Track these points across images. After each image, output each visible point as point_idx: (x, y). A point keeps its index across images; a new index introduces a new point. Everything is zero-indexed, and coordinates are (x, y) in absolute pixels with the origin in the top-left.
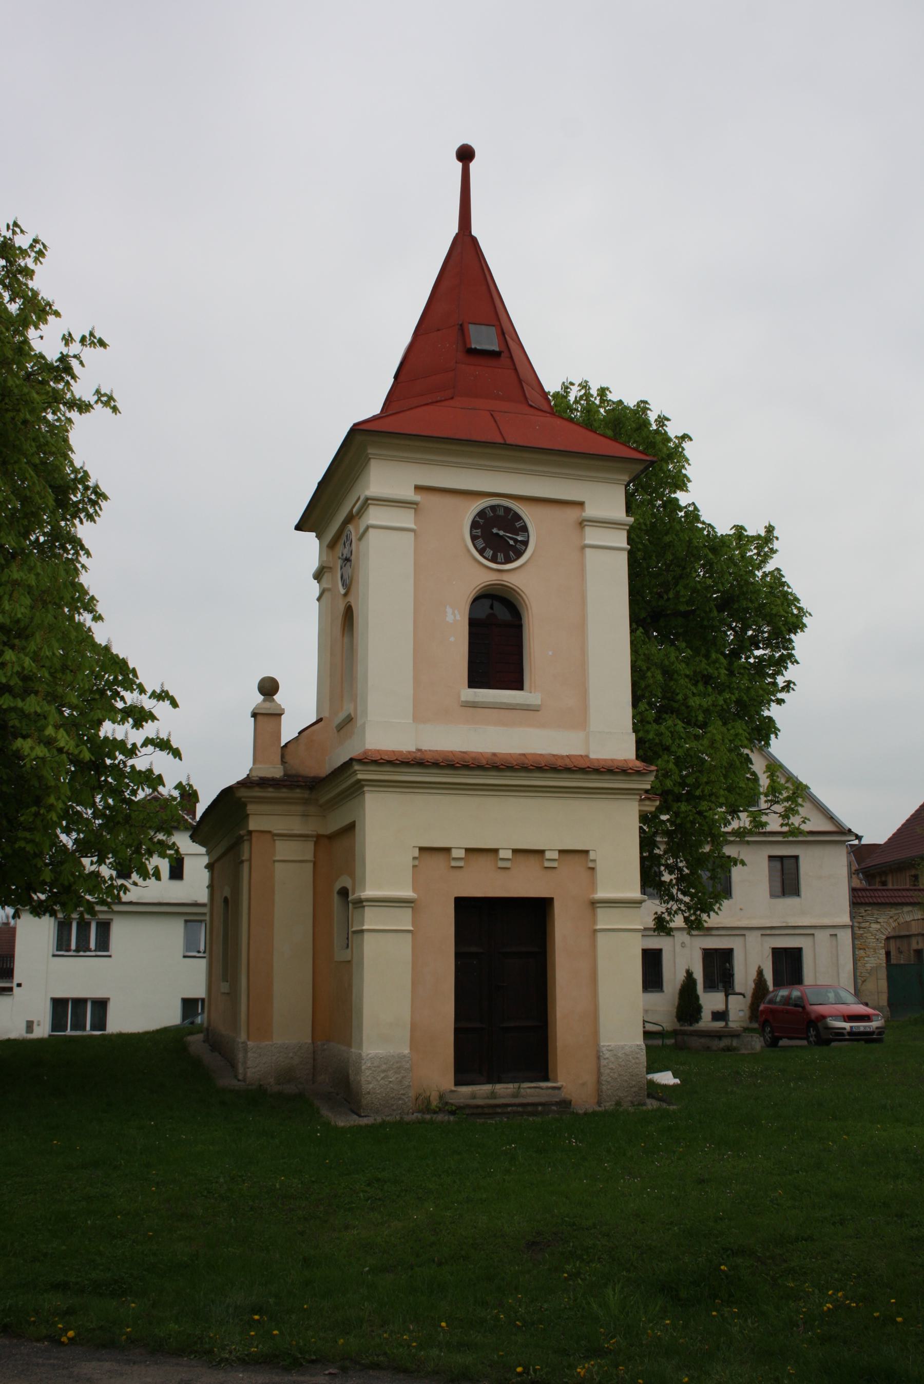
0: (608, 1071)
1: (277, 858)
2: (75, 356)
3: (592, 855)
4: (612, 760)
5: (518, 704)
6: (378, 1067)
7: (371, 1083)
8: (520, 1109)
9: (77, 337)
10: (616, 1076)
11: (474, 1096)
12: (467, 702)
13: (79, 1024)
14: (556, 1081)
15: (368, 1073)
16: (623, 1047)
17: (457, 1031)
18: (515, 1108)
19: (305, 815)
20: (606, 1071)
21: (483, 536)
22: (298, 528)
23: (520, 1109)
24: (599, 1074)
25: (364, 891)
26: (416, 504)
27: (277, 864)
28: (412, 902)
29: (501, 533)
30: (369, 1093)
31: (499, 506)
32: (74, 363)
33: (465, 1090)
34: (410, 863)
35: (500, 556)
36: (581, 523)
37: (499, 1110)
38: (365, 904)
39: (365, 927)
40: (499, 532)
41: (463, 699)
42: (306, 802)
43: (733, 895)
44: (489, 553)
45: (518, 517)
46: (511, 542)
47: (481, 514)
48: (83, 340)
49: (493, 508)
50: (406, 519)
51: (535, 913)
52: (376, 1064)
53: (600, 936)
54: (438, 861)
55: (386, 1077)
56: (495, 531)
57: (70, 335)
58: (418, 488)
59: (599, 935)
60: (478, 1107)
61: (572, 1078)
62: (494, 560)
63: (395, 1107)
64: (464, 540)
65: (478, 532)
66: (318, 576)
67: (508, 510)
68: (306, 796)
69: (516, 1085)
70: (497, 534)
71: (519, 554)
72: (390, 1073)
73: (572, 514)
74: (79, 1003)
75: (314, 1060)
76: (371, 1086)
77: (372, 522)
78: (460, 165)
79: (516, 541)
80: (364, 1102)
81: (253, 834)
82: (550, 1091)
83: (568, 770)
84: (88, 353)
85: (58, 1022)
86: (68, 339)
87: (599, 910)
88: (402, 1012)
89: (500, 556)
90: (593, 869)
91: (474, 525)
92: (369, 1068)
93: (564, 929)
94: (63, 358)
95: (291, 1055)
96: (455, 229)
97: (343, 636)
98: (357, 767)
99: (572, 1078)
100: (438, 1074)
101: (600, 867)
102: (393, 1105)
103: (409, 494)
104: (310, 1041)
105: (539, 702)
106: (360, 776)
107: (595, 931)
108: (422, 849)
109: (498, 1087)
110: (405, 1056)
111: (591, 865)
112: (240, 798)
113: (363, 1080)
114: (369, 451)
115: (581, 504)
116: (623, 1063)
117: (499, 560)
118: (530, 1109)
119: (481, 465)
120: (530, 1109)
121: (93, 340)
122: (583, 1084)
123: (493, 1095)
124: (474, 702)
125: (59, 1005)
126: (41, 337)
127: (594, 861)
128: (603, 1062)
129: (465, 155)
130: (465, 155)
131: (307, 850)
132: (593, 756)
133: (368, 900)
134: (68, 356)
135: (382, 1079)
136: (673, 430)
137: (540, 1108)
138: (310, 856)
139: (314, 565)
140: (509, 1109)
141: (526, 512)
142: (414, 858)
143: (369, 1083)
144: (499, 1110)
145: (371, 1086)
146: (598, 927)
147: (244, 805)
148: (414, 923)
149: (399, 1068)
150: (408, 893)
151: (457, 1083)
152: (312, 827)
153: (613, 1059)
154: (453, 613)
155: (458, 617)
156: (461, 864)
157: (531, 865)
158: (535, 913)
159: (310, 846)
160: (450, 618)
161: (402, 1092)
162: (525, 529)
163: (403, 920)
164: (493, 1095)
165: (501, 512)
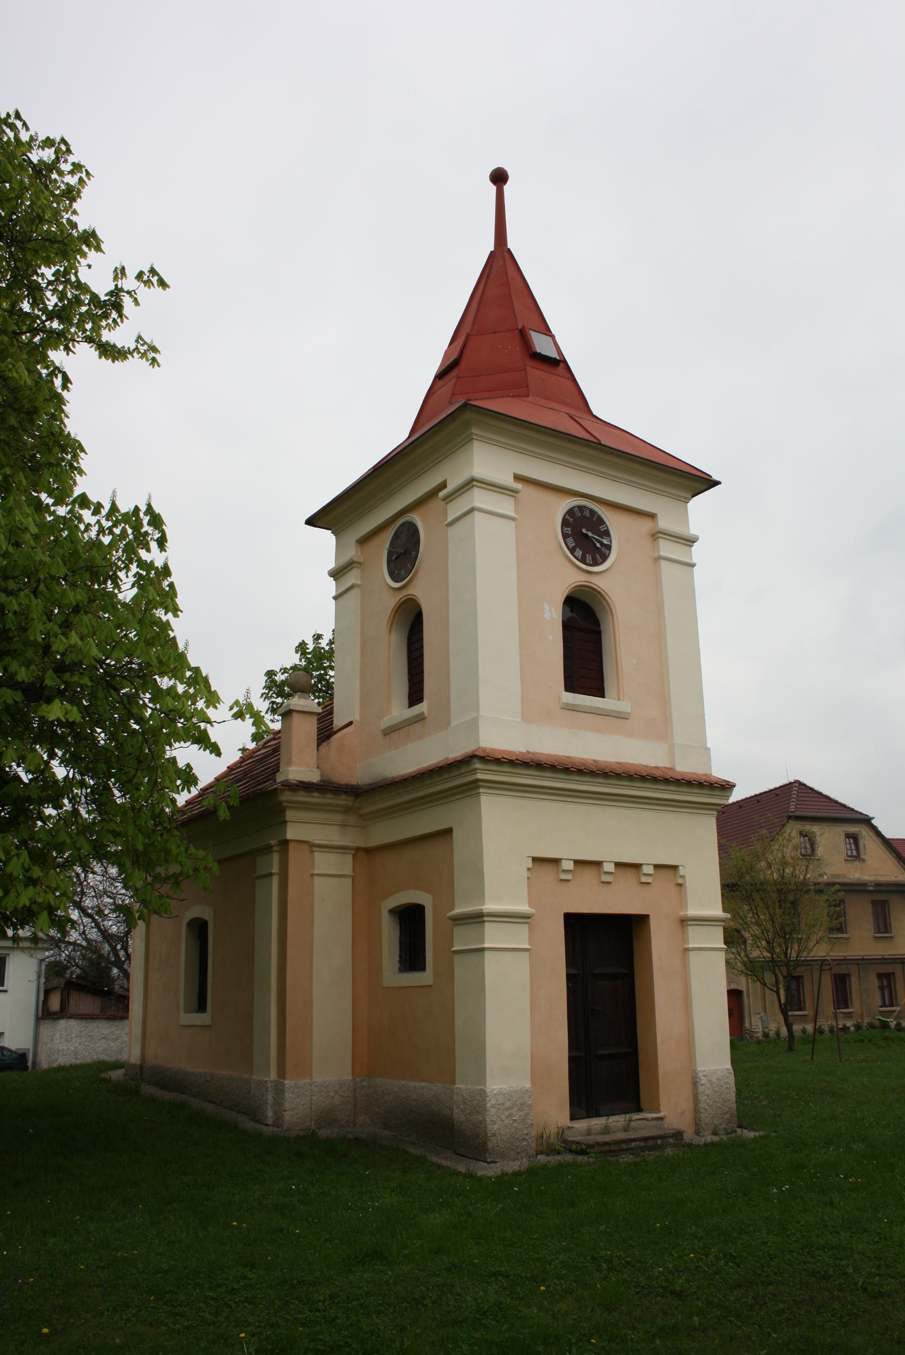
0: (705, 1097)
1: (316, 872)
2: (129, 292)
3: (681, 871)
5: (611, 710)
6: (503, 1104)
7: (497, 1124)
8: (642, 1144)
9: (132, 273)
10: (711, 1103)
12: (567, 704)
14: (659, 1111)
15: (493, 1111)
16: (715, 1072)
17: (571, 1059)
18: (638, 1143)
19: (344, 825)
20: (703, 1098)
21: (573, 535)
23: (642, 1144)
24: (696, 1100)
25: (484, 904)
26: (516, 492)
27: (315, 878)
28: (528, 918)
29: (590, 534)
30: (494, 1134)
31: (585, 507)
32: (127, 301)
33: (581, 1125)
34: (526, 874)
35: (589, 558)
36: (653, 535)
37: (624, 1146)
38: (485, 919)
39: (486, 945)
41: (564, 700)
42: (347, 810)
44: (579, 553)
45: (601, 522)
46: (598, 545)
47: (570, 512)
48: (140, 276)
49: (581, 508)
50: (505, 505)
52: (500, 1101)
53: (693, 956)
54: (547, 872)
55: (511, 1115)
56: (584, 531)
57: (123, 269)
58: (518, 478)
59: (692, 954)
62: (583, 560)
63: (519, 1150)
64: (557, 537)
65: (568, 530)
66: (336, 574)
67: (593, 512)
68: (350, 803)
69: (628, 1116)
70: (586, 535)
71: (605, 558)
72: (514, 1111)
73: (645, 525)
75: (355, 1098)
76: (496, 1126)
77: (477, 504)
78: (493, 188)
79: (602, 544)
80: (490, 1145)
81: (291, 844)
82: (654, 1122)
84: (143, 292)
86: (120, 273)
87: (690, 928)
88: (513, 1039)
89: (589, 558)
90: (680, 885)
91: (565, 523)
92: (493, 1107)
93: (660, 945)
94: (116, 293)
95: (332, 1094)
96: (489, 245)
97: (390, 632)
98: (478, 765)
100: (554, 1110)
101: (689, 883)
102: (517, 1147)
103: (510, 482)
104: (350, 1078)
105: (629, 710)
106: (480, 776)
107: (686, 950)
108: (535, 860)
109: (612, 1119)
110: (527, 1090)
111: (680, 881)
112: (281, 803)
113: (488, 1120)
114: (474, 431)
116: (716, 1089)
117: (588, 561)
118: (650, 1143)
119: (575, 464)
120: (650, 1143)
121: (152, 278)
122: (683, 1113)
123: (606, 1130)
124: (574, 705)
126: (89, 266)
127: (683, 877)
128: (701, 1089)
129: (499, 178)
130: (499, 178)
131: (344, 864)
132: (678, 769)
133: (490, 915)
134: (121, 290)
135: (507, 1118)
137: (659, 1141)
138: (348, 871)
139: (331, 563)
140: (633, 1144)
142: (529, 869)
143: (494, 1123)
144: (624, 1146)
145: (496, 1126)
146: (691, 946)
147: (283, 810)
148: (531, 940)
149: (521, 1104)
150: (523, 907)
151: (573, 1118)
152: (352, 839)
153: (708, 1085)
154: (550, 611)
155: (555, 616)
156: (569, 877)
157: (627, 880)
159: (349, 859)
160: (547, 615)
161: (526, 1131)
162: (607, 533)
163: (518, 936)
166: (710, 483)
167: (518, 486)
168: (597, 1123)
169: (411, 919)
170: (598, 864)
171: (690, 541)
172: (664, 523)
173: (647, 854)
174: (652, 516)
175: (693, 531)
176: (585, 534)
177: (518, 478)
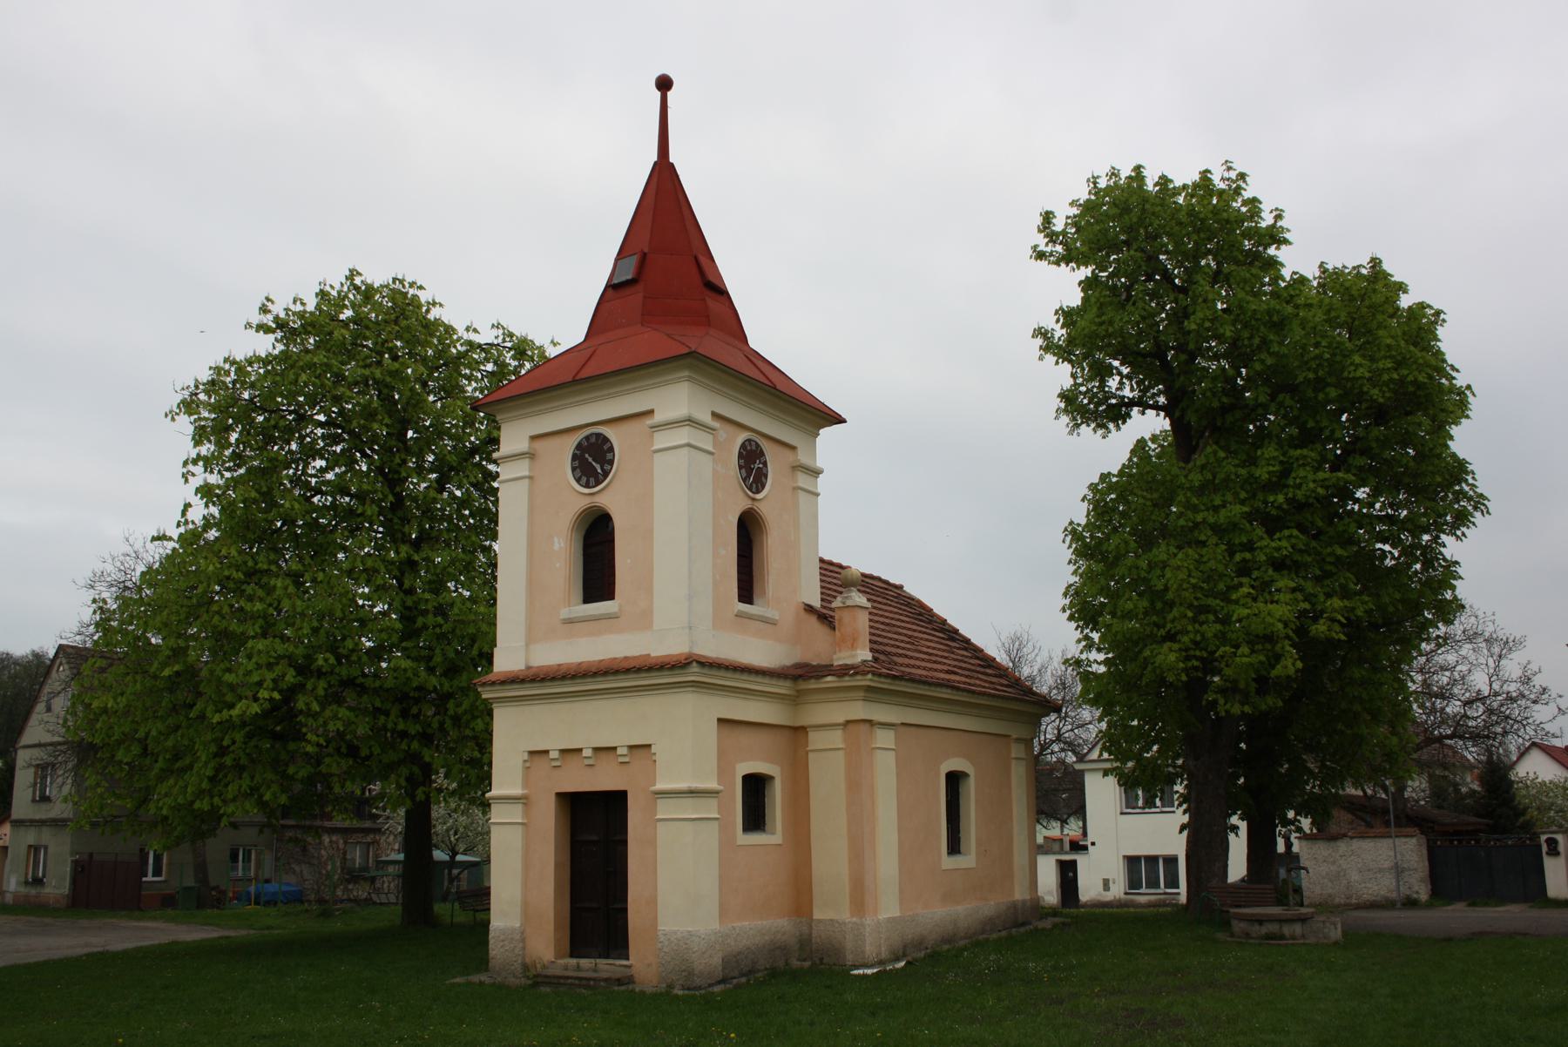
4: (626, 658)
11: (566, 968)
13: (1153, 883)
22: (844, 421)
40: (593, 458)
43: (553, 798)
49: (587, 438)
51: (615, 802)
58: (715, 415)
60: (580, 979)
61: (644, 961)
67: (598, 435)
74: (1152, 860)
83: (627, 671)
85: (1134, 883)
89: (584, 479)
96: (655, 158)
99: (644, 961)
103: (707, 418)
108: (532, 753)
115: (651, 412)
125: (1132, 862)
129: (664, 84)
130: (664, 84)
136: (1083, 194)
141: (607, 431)
158: (615, 802)
160: (556, 547)
164: (578, 968)
165: (593, 440)
166: (840, 420)
167: (716, 424)
168: (585, 963)
169: (755, 818)
170: (547, 752)
171: (816, 473)
172: (803, 457)
173: (620, 738)
174: (793, 448)
175: (819, 464)
176: (752, 465)
177: (715, 415)
